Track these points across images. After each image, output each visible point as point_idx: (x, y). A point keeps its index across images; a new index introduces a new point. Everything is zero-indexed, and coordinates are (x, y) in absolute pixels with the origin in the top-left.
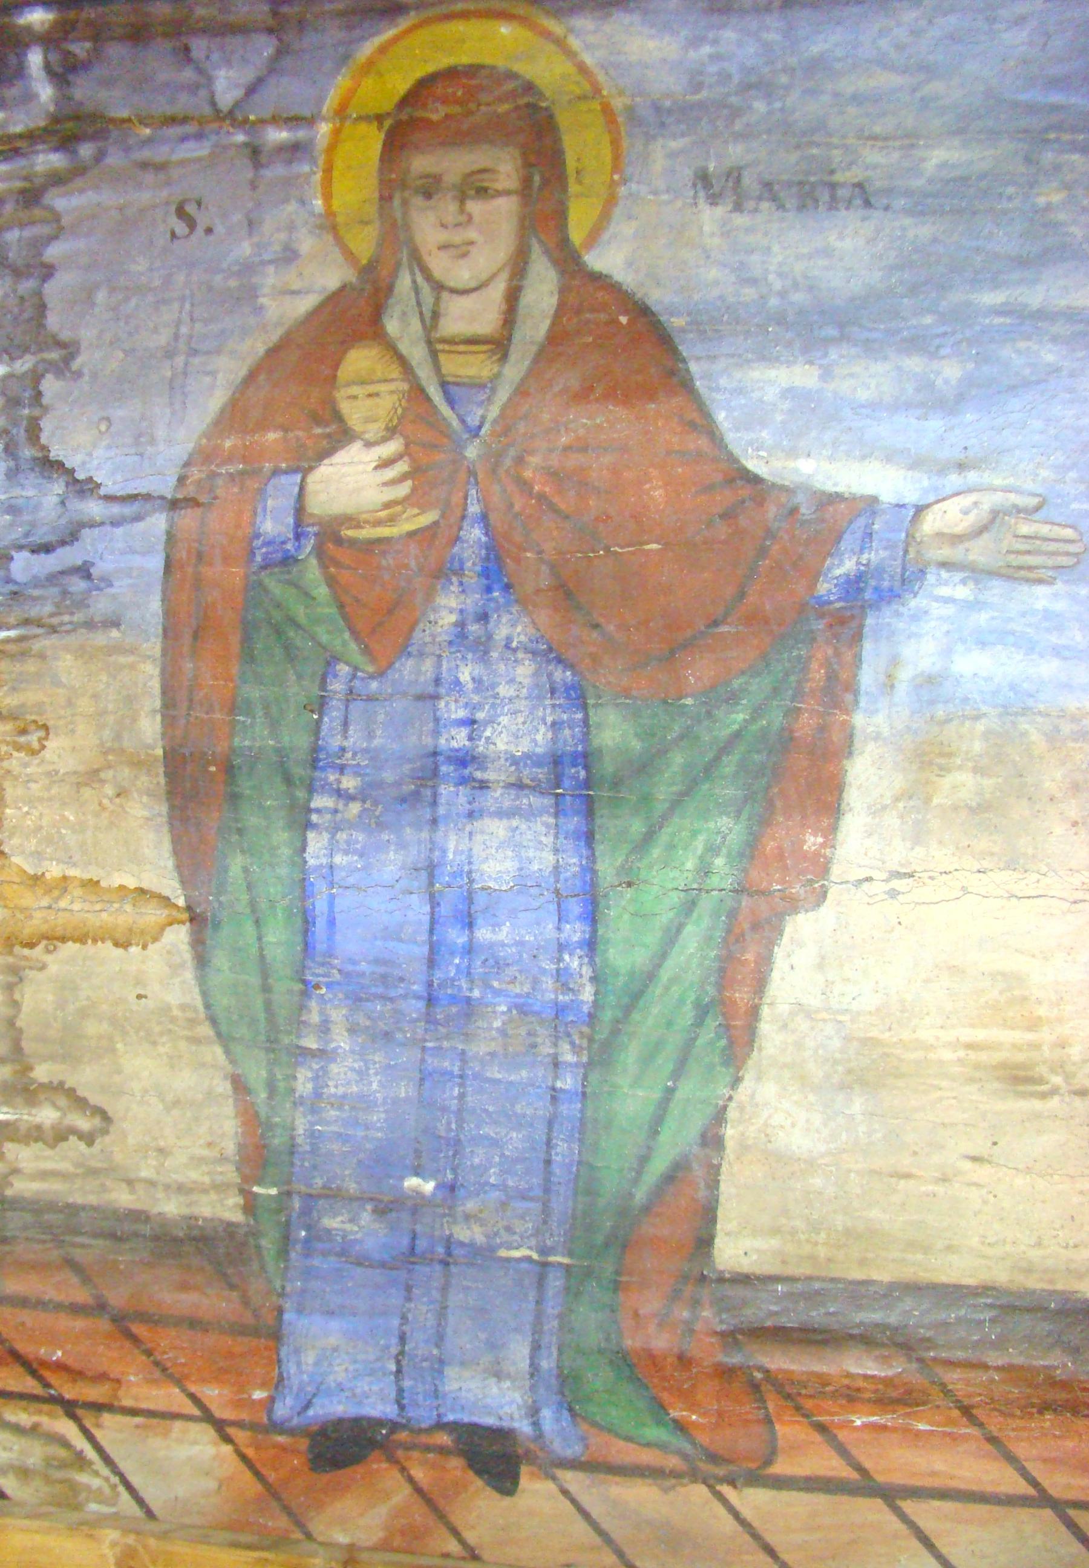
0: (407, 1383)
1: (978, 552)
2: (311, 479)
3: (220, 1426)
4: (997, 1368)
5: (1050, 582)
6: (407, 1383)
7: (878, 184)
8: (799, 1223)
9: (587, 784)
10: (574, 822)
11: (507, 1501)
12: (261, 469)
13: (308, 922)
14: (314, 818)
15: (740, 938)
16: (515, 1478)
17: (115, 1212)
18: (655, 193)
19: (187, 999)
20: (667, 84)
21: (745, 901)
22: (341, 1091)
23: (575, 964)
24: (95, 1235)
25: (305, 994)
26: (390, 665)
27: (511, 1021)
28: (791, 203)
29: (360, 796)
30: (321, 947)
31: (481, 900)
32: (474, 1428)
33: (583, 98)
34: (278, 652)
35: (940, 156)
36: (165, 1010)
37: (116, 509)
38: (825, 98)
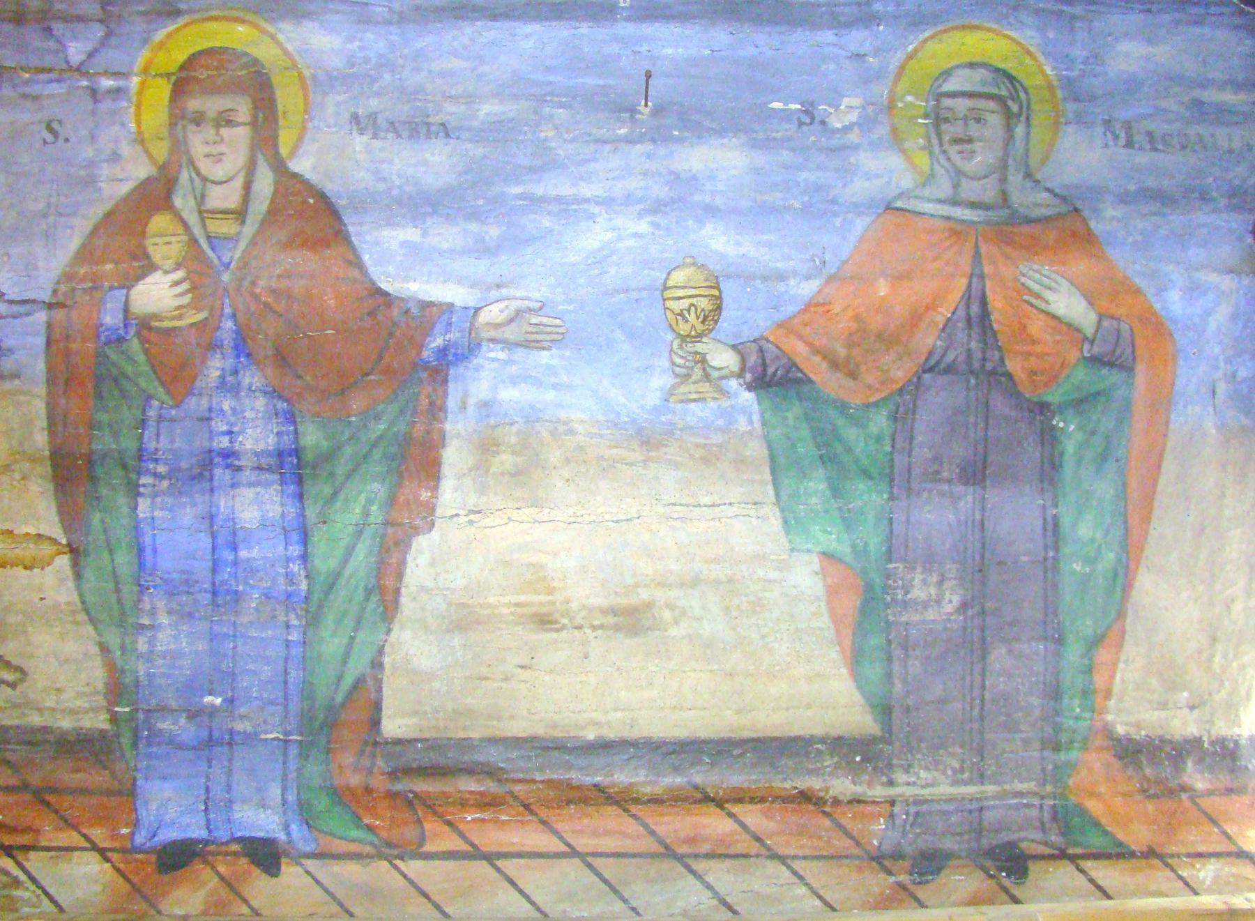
0: (212, 816)
1: (510, 333)
2: (133, 292)
3: (102, 852)
4: (542, 782)
5: (549, 349)
6: (212, 816)
7: (453, 124)
8: (427, 708)
9: (299, 466)
10: (292, 488)
11: (274, 880)
12: (102, 286)
13: (140, 551)
14: (142, 490)
15: (388, 550)
16: (278, 866)
17: (32, 728)
18: (328, 126)
19: (70, 599)
20: (336, 62)
21: (390, 530)
22: (164, 648)
23: (296, 569)
24: (19, 743)
25: (141, 592)
26: (182, 401)
27: (261, 603)
28: (405, 134)
29: (169, 476)
30: (149, 565)
31: (240, 535)
32: (252, 840)
33: (287, 68)
34: (116, 392)
35: (488, 109)
36: (57, 605)
37: (16, 309)
38: (424, 73)
